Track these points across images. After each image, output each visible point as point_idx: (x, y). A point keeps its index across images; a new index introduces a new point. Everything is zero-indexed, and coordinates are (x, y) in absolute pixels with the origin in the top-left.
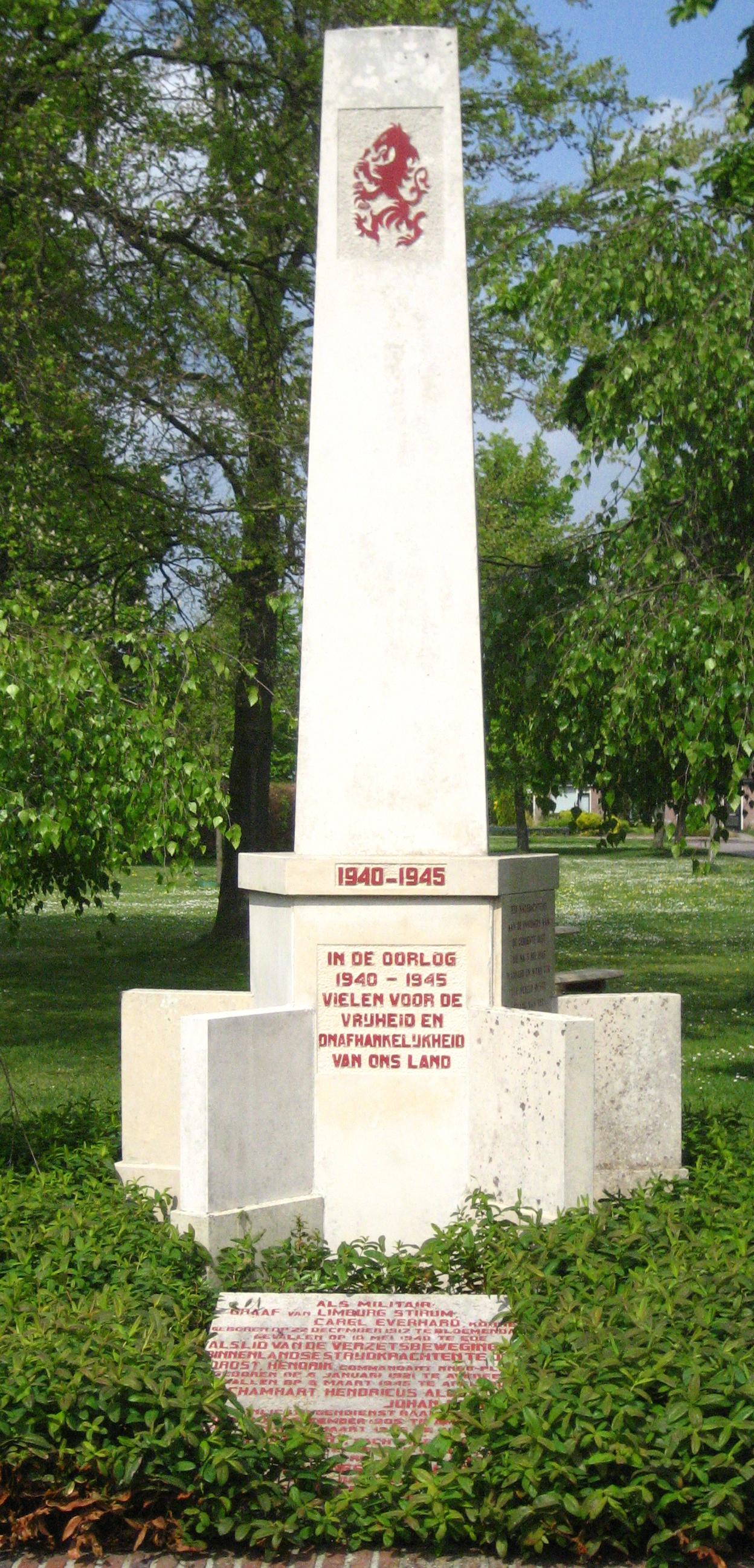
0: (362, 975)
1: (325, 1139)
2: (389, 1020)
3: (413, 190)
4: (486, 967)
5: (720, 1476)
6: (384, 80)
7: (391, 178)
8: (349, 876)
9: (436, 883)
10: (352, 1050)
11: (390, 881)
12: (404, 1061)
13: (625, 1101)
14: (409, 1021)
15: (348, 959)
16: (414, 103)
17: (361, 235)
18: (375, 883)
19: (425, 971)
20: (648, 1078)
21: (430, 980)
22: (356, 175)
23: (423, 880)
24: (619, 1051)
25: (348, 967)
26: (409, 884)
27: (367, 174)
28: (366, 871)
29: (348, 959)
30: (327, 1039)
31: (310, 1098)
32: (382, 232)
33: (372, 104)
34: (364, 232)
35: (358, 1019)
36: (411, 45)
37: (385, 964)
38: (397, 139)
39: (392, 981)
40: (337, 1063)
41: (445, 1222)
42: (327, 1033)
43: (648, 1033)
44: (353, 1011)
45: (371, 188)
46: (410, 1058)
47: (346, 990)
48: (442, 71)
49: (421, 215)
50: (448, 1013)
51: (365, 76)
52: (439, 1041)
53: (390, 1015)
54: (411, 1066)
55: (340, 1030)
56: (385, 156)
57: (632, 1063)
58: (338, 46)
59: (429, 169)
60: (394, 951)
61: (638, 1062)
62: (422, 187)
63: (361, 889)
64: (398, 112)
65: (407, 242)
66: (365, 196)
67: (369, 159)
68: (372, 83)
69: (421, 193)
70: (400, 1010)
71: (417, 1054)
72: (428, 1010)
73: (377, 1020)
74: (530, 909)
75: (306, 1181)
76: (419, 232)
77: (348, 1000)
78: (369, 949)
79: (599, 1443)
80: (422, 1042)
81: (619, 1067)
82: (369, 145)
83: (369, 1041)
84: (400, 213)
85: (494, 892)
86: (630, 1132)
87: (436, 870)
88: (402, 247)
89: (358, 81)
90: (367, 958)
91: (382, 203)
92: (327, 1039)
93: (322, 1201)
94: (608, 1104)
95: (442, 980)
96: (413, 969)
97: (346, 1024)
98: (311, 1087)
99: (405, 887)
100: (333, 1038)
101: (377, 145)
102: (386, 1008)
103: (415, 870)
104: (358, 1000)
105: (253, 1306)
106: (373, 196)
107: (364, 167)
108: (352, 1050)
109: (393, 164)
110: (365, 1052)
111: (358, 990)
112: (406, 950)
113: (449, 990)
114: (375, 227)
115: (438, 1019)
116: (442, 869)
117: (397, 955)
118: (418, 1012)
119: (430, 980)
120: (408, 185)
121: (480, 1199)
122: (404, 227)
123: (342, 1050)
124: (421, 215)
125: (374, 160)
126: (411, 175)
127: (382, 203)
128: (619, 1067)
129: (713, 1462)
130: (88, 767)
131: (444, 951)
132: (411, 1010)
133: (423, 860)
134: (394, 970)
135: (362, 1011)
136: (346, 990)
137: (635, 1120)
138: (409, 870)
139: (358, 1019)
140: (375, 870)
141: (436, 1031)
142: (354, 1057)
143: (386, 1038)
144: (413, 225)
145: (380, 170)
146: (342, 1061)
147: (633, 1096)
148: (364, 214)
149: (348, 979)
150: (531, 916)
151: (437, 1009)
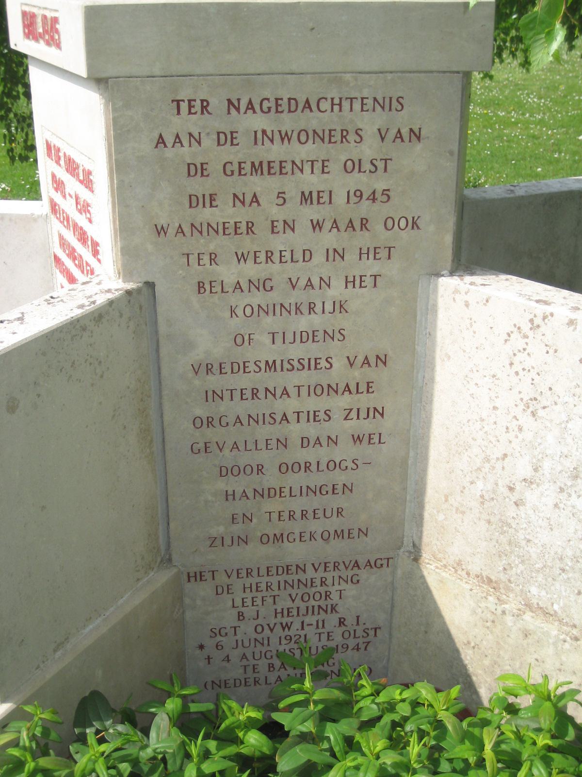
13: (531, 496)
86: (533, 551)
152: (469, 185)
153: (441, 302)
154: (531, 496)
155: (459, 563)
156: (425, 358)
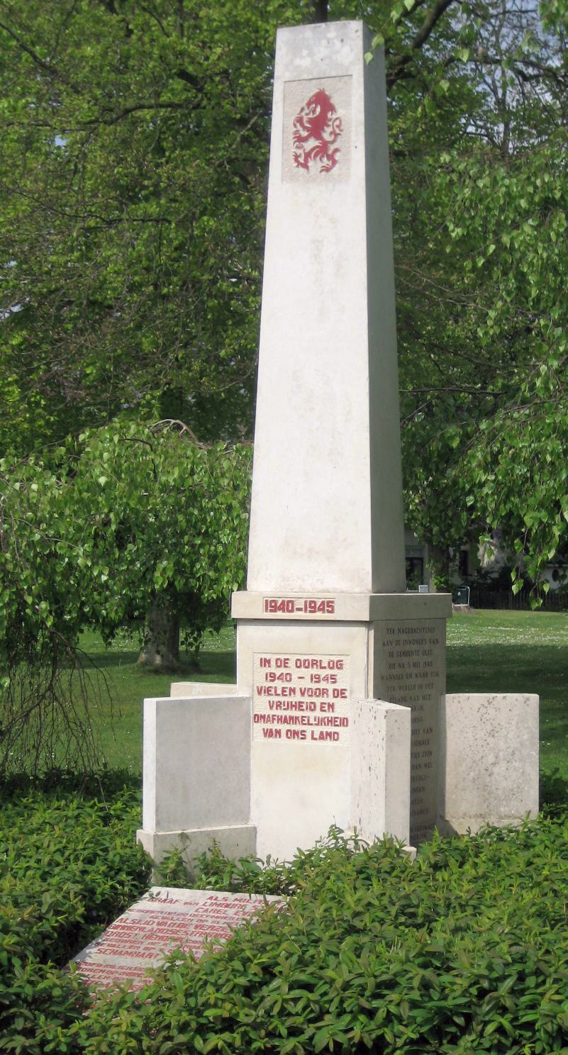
0: (282, 674)
1: (258, 787)
2: (299, 706)
3: (331, 133)
4: (362, 672)
5: (294, 1032)
6: (322, 62)
7: (316, 127)
8: (272, 605)
9: (328, 612)
10: (275, 726)
11: (299, 609)
12: (308, 735)
13: (496, 770)
14: (312, 707)
15: (273, 663)
16: (333, 74)
17: (297, 166)
18: (289, 611)
19: (323, 673)
20: (513, 754)
21: (326, 679)
22: (295, 126)
23: (319, 610)
24: (492, 734)
25: (273, 669)
26: (311, 612)
27: (302, 125)
28: (283, 602)
29: (273, 663)
30: (258, 718)
31: (247, 759)
32: (311, 163)
33: (305, 77)
34: (299, 164)
35: (279, 705)
36: (332, 34)
37: (297, 667)
38: (322, 100)
39: (301, 679)
40: (265, 735)
41: (308, 846)
42: (259, 713)
43: (513, 723)
44: (276, 699)
45: (304, 134)
46: (313, 732)
47: (271, 684)
48: (352, 50)
49: (336, 150)
50: (338, 702)
51: (303, 57)
52: (331, 721)
53: (300, 702)
54: (313, 738)
55: (268, 712)
56: (314, 112)
57: (501, 743)
58: (285, 38)
59: (343, 118)
60: (303, 658)
61: (506, 742)
62: (338, 131)
63: (280, 615)
64: (323, 81)
65: (327, 169)
66: (300, 139)
67: (303, 114)
68: (305, 62)
69: (336, 135)
70: (306, 699)
71: (318, 730)
72: (325, 700)
73: (291, 706)
74: (412, 631)
75: (245, 816)
76: (334, 162)
77: (273, 692)
78: (286, 657)
79: (212, 1001)
80: (320, 722)
81: (492, 745)
82: (304, 104)
83: (285, 720)
84: (323, 150)
85: (367, 618)
86: (500, 792)
87: (328, 602)
88: (323, 173)
89: (298, 62)
90: (285, 663)
91: (312, 143)
92: (258, 718)
93: (255, 829)
94: (483, 772)
95: (333, 679)
96: (315, 671)
97: (271, 707)
98: (248, 751)
99: (308, 614)
100: (263, 717)
101: (309, 104)
102: (297, 698)
103: (315, 602)
104: (279, 692)
105: (163, 897)
106: (305, 139)
107: (300, 120)
108: (275, 726)
109: (319, 117)
110: (284, 728)
111: (279, 684)
112: (310, 658)
113: (338, 686)
114: (306, 160)
115: (331, 706)
116: (332, 602)
117: (305, 661)
118: (318, 701)
119: (326, 679)
120: (328, 130)
121: (335, 831)
122: (325, 159)
123: (268, 726)
124: (336, 150)
125: (307, 114)
126: (330, 123)
127: (312, 143)
128: (492, 745)
129: (290, 1021)
130: (199, 534)
131: (335, 659)
132: (314, 699)
133: (320, 595)
134: (302, 672)
135: (282, 699)
136: (271, 684)
137: (504, 784)
138: (311, 602)
139: (279, 705)
140: (288, 602)
141: (329, 715)
142: (276, 731)
143: (297, 718)
144: (331, 158)
145: (310, 121)
146: (269, 733)
147: (503, 765)
148: (299, 152)
149: (272, 677)
150: (416, 636)
151: (331, 700)
152: (136, 196)
153: (447, 704)
154: (496, 770)
155: (465, 814)
156: (517, 832)
